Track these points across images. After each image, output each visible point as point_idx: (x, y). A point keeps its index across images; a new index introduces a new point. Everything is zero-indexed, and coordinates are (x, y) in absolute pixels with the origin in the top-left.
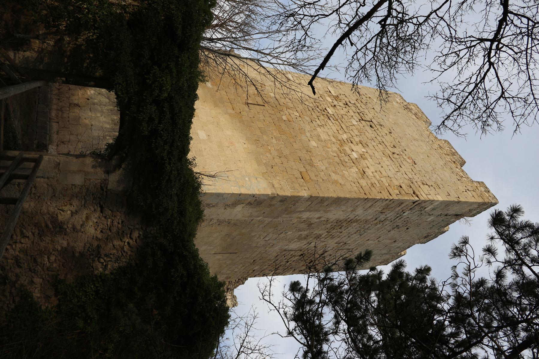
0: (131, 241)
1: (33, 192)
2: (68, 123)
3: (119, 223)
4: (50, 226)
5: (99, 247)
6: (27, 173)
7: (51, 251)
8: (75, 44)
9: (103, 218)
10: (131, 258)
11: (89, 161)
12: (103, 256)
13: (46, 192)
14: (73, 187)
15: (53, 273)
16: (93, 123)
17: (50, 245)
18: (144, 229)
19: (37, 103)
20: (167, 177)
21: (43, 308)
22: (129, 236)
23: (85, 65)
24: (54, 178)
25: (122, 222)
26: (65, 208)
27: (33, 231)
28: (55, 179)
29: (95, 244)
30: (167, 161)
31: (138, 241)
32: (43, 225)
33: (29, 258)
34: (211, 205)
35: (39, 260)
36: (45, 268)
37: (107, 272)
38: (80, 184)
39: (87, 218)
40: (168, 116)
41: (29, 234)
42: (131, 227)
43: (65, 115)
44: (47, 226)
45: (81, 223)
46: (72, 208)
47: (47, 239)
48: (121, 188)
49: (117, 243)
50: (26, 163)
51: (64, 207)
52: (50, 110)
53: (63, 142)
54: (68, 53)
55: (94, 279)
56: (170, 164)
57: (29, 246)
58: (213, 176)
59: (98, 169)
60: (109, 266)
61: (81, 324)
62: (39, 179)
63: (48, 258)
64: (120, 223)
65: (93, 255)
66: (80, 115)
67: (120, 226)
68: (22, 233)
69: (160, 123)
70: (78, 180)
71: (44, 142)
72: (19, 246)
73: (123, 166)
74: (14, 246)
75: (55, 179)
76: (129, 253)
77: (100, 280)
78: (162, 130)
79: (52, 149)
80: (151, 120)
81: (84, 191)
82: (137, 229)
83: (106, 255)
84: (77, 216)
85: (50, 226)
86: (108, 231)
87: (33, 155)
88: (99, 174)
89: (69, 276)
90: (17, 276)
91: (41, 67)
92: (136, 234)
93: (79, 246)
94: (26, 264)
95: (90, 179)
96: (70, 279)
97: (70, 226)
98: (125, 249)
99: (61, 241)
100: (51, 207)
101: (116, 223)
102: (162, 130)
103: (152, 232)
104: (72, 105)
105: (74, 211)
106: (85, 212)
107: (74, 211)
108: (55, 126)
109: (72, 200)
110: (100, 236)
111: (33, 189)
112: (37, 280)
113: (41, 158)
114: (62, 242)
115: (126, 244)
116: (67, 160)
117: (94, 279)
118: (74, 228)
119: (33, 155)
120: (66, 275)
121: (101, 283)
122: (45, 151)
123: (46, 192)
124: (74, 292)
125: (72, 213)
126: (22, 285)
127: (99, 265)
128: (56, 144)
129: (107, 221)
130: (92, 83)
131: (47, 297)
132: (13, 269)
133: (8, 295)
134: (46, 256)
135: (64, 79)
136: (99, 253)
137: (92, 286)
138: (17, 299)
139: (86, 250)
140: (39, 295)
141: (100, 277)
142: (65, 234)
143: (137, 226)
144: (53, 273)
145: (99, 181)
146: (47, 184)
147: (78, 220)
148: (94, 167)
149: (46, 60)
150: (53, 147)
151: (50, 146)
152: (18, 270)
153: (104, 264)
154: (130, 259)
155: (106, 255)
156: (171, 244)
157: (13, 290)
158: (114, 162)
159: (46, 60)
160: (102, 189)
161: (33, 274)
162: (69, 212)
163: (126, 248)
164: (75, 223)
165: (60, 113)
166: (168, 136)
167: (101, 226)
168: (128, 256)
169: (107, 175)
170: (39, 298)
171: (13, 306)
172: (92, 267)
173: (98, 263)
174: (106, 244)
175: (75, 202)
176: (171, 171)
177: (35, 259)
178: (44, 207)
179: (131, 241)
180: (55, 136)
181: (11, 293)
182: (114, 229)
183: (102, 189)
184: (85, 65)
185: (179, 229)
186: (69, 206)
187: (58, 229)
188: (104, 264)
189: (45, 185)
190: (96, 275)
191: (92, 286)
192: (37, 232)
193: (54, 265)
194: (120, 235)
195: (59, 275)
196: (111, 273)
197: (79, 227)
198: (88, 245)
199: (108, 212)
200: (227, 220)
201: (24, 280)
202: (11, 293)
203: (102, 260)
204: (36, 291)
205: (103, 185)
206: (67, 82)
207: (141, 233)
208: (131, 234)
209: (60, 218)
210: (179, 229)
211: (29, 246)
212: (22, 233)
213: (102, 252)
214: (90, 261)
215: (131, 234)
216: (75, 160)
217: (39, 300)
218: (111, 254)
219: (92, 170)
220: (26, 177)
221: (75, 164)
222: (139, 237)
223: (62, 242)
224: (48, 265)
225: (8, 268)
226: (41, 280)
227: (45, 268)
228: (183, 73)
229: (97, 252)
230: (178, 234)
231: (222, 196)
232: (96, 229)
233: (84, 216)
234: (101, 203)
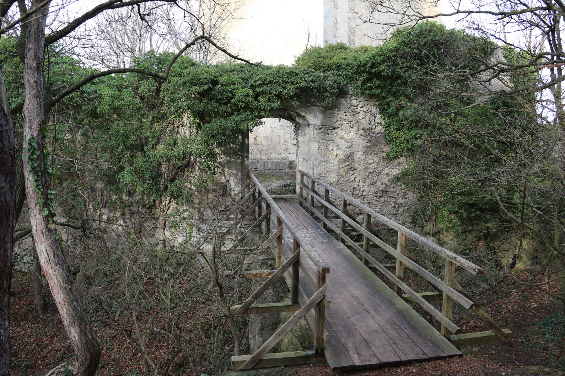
0: (360, 106)
1: (324, 175)
2: (270, 146)
3: (346, 115)
4: (348, 163)
5: (363, 129)
6: (310, 181)
7: (365, 162)
8: (221, 154)
9: (342, 127)
10: (373, 105)
11: (300, 139)
12: (371, 126)
13: (324, 167)
14: (319, 149)
15: (381, 161)
16: (269, 126)
17: (361, 163)
18: (351, 96)
19: (257, 169)
20: (311, 83)
21: (406, 166)
22: (355, 107)
23: (234, 146)
24: (314, 162)
25: (345, 113)
26: (335, 154)
27: (351, 174)
28: (315, 161)
29: (361, 132)
30: (298, 85)
31: (359, 100)
32: (347, 168)
33: (370, 177)
34: (335, 22)
35: (372, 170)
36: (378, 166)
37: (383, 122)
38: (317, 144)
39: (342, 138)
40: (265, 88)
41: (353, 176)
42: (349, 106)
43: (265, 148)
44: (348, 166)
45: (345, 142)
46: (335, 149)
47: (357, 165)
48: (320, 115)
49: (361, 116)
50: (304, 181)
51: (334, 155)
52: (262, 160)
53: (287, 150)
54: (228, 158)
55: (387, 132)
56: (301, 83)
57: (361, 177)
58: (309, 35)
59: (307, 132)
60: (379, 121)
61: (419, 142)
62: (315, 172)
63: (370, 164)
64: (346, 114)
65: (369, 133)
66: (263, 136)
67: (348, 114)
68: (352, 182)
69: (271, 93)
70: (315, 146)
71: (288, 163)
72: (361, 183)
73: (303, 114)
74: (361, 186)
75: (315, 161)
76: (369, 106)
77: (388, 128)
78: (276, 91)
79: (292, 158)
80: (269, 100)
81: (322, 141)
82: (350, 101)
83: (370, 123)
84: (341, 146)
85: (348, 163)
86: (352, 123)
87: (298, 176)
88: (311, 132)
89: (384, 150)
90: (382, 184)
91: (240, 174)
92: (355, 102)
93: (363, 143)
94: (374, 178)
95: (314, 138)
96: (387, 149)
97: (348, 150)
98: (366, 110)
99: (359, 156)
100: (334, 163)
101: (346, 118)
102: (276, 91)
103: (353, 90)
104: (256, 142)
105: (337, 147)
106: (338, 140)
107: (337, 147)
108: (274, 156)
109: (329, 149)
110: (356, 129)
111: (322, 175)
112: (386, 171)
113: (299, 171)
114: (359, 156)
115: (362, 109)
116: (301, 153)
117: (387, 132)
118: (350, 147)
119: (298, 176)
120: (383, 152)
121: (391, 127)
122: (294, 163)
123: (324, 167)
124: (396, 146)
125: (338, 149)
126: (389, 181)
127: (378, 128)
128: (288, 155)
129: (344, 124)
130: (246, 140)
131: (399, 164)
132: (377, 187)
133: (395, 189)
134: (369, 165)
135: (245, 159)
136: (368, 129)
137: (393, 133)
138: (399, 184)
139: (366, 138)
140: (397, 170)
141: (386, 127)
142: (354, 153)
143: (348, 101)
144: (381, 161)
145: (315, 131)
146: (318, 166)
147: (343, 145)
148: (305, 135)
149: (234, 172)
150: (291, 157)
151: (290, 159)
152: (378, 184)
153: (376, 125)
154: (374, 106)
155: (370, 123)
156: (363, 75)
157: (392, 186)
158: (301, 121)
159: (234, 172)
160: (321, 128)
161: (382, 174)
162: (338, 151)
163: (365, 109)
164: (346, 146)
165: (263, 152)
166: (280, 86)
167: (348, 128)
168: (371, 108)
169: (311, 126)
170: (399, 170)
171: (403, 186)
172: (378, 133)
173: (376, 129)
174: (362, 124)
175: (331, 147)
176: (306, 81)
177: (371, 173)
178: (334, 168)
179: (360, 106)
180: (282, 156)
181: (394, 188)
182: (351, 118)
183: (321, 128)
184: (234, 146)
185: (351, 69)
186: (333, 152)
187: (350, 158)
188: (376, 125)
189: (319, 168)
190: (385, 131)
191: (393, 133)
192: (351, 172)
193: (376, 160)
194: (355, 114)
195: (383, 157)
196: (384, 119)
197: (349, 144)
198: (362, 137)
199: (337, 124)
200: (350, 3)
201: (386, 180)
202: (394, 188)
203: (374, 127)
204: (394, 171)
205: (318, 128)
206: (247, 157)
207: (354, 98)
208: (354, 106)
209: (342, 157)
210: (351, 69)
211: (361, 177)
212: (352, 182)
213: (368, 126)
214: (374, 135)
215: (354, 106)
216: (300, 149)
217: (401, 170)
218: (369, 120)
219: (307, 136)
220: (313, 182)
221: (303, 148)
222: (356, 100)
223: (359, 156)
224: (375, 164)
225: (376, 189)
226: (386, 168)
227: (378, 166)
228: (233, 80)
229: (368, 131)
230: (354, 70)
231: (327, 13)
232: (350, 132)
233: (341, 140)
234: (331, 129)
